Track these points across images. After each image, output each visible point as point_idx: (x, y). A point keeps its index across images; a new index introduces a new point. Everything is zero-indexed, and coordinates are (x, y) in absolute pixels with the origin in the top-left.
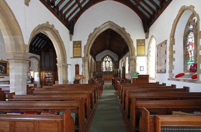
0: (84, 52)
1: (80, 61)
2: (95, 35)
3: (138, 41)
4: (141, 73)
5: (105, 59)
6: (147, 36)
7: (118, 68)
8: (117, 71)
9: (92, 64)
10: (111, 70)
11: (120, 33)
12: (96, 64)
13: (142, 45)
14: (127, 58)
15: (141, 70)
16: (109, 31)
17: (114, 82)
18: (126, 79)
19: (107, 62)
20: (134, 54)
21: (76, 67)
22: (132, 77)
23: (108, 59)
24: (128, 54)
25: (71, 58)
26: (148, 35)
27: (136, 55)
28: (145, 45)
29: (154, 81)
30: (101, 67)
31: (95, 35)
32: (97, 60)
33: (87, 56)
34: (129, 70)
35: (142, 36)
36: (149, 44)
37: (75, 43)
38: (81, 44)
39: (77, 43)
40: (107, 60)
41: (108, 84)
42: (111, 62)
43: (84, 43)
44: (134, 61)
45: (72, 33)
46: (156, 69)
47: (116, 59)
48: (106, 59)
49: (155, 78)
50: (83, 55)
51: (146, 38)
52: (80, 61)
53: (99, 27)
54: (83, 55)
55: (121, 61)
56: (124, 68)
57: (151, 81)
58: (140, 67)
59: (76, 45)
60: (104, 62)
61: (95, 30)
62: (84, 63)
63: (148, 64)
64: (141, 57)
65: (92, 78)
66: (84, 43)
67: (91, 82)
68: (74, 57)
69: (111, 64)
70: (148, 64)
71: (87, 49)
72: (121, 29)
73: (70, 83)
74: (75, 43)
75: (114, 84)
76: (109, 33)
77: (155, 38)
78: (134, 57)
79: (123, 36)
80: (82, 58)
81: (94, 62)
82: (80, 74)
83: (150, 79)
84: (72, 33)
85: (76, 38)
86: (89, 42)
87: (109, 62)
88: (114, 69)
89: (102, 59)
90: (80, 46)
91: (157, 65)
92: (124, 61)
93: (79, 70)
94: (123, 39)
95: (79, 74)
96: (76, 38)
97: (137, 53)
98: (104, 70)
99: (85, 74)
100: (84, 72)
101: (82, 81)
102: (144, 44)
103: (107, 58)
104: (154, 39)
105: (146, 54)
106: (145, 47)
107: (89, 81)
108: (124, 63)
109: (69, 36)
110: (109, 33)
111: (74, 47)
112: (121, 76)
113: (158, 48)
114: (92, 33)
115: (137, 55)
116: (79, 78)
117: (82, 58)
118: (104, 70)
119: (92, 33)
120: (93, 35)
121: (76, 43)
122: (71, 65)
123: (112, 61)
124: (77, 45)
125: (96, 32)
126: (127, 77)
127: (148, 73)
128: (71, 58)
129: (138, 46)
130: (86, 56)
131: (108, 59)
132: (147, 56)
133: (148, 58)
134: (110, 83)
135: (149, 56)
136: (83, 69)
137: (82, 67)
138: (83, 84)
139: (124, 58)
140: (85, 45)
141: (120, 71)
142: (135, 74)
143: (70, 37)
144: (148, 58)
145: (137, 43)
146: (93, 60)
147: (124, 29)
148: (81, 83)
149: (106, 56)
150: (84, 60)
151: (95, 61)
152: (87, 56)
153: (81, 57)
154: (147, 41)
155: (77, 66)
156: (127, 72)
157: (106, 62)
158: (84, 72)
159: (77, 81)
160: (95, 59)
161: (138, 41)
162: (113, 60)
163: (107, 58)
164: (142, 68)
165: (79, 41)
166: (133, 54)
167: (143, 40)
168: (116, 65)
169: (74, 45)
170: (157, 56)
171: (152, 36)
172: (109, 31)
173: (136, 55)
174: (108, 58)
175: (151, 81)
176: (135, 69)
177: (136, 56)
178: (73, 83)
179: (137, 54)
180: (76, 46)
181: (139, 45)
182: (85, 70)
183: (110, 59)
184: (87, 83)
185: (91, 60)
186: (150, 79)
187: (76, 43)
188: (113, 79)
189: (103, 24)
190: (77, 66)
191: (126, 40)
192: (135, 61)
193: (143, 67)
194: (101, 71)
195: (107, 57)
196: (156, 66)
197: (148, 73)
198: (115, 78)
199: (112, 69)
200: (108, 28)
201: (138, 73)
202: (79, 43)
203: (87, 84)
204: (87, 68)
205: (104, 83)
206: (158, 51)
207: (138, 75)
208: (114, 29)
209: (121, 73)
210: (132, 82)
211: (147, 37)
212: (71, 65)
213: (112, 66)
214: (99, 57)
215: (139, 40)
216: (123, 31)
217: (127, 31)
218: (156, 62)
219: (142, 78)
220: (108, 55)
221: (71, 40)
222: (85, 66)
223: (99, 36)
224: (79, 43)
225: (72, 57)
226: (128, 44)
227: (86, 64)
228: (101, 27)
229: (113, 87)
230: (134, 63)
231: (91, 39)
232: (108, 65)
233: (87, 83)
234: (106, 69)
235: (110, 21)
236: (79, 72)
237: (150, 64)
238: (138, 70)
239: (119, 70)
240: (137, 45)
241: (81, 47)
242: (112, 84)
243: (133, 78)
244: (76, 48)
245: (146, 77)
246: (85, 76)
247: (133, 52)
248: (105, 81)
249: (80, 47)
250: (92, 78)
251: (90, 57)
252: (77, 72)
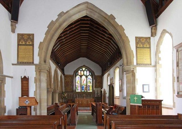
0: (39, 55)
1: (30, 72)
2: (60, 26)
3: (138, 40)
4: (149, 96)
5: (79, 72)
6: (153, 31)
7: (101, 87)
8: (99, 92)
9: (57, 79)
10: (89, 90)
11: (106, 25)
12: (65, 79)
13: (145, 48)
14: (117, 71)
15: (145, 90)
16: (88, 20)
17: (94, 110)
18: (116, 106)
19: (84, 77)
20: (131, 62)
21: (22, 81)
22: (131, 104)
23: (85, 72)
24: (118, 64)
25: (13, 64)
26: (156, 29)
27: (135, 64)
28: (150, 48)
29: (173, 113)
30: (73, 85)
31: (60, 26)
32: (66, 73)
33: (45, 62)
34: (121, 90)
35: (145, 31)
36: (158, 46)
37: (21, 37)
38: (33, 40)
39: (26, 38)
40: (82, 74)
41: (85, 113)
42: (90, 77)
43: (39, 39)
44: (131, 74)
45: (15, 17)
46: (174, 90)
47: (98, 73)
48: (82, 72)
49: (174, 106)
50: (37, 61)
51: (152, 36)
52: (30, 72)
53: (67, 12)
54: (37, 61)
55: (105, 76)
56: (111, 88)
57: (165, 112)
58: (143, 85)
59: (24, 40)
60: (79, 71)
61: (61, 15)
62: (40, 75)
63: (156, 81)
64: (104, 85)
65: (57, 102)
66: (39, 39)
67: (53, 111)
68: (19, 63)
69: (90, 80)
70: (156, 81)
71: (44, 50)
72: (107, 17)
73: (9, 111)
74: (21, 37)
75: (95, 114)
76: (86, 27)
77: (170, 34)
78: (132, 67)
79: (111, 30)
80: (34, 67)
81: (61, 76)
82: (31, 94)
83: (164, 107)
84: (15, 17)
85: (23, 28)
86: (49, 37)
87: (87, 77)
88: (94, 89)
89: (74, 72)
90: (31, 43)
91: (178, 81)
92: (112, 76)
93: (28, 88)
94: (110, 35)
95: (27, 95)
96: (23, 28)
97: (137, 60)
98: (79, 90)
99: (40, 96)
100: (38, 91)
101: (35, 110)
102: (148, 46)
103: (84, 71)
104: (167, 36)
105: (153, 63)
106: (150, 51)
107: (49, 109)
108: (112, 80)
109: (9, 23)
110: (86, 27)
111: (18, 45)
112: (107, 101)
113: (177, 51)
114: (54, 20)
115: (137, 64)
116: (27, 103)
117: (36, 65)
118: (79, 90)
119: (54, 20)
120: (57, 24)
121: (24, 37)
122: (12, 77)
123: (92, 76)
124: (26, 42)
125: (61, 20)
126: (117, 102)
127: (156, 97)
128: (13, 64)
129: (139, 48)
130: (43, 63)
131: (85, 72)
132: (155, 66)
133: (156, 70)
134: (88, 111)
135: (157, 68)
136: (36, 85)
137: (36, 81)
138: (36, 116)
139: (112, 70)
140: (41, 43)
141: (105, 91)
142: (136, 98)
143: (12, 25)
144: (156, 70)
145: (137, 43)
146: (59, 73)
147: (112, 17)
148: (33, 113)
149: (81, 67)
150: (39, 70)
151: (64, 74)
152: (45, 62)
153: (32, 63)
154: (154, 41)
155: (25, 80)
156: (117, 93)
157: (81, 76)
158: (38, 91)
159: (22, 110)
160: (63, 71)
161: (138, 40)
162: (92, 74)
163: (84, 71)
164: (146, 87)
165: (29, 35)
166: (129, 63)
167: (146, 38)
168: (98, 81)
169: (19, 41)
170: (178, 66)
171: (164, 31)
172: (88, 20)
173: (135, 64)
174: (85, 70)
175: (165, 112)
176: (134, 88)
177: (135, 67)
178: (15, 114)
179: (137, 62)
180: (24, 43)
181: (141, 48)
182: (40, 87)
183: (88, 72)
184: (44, 113)
185: (56, 71)
186: (164, 107)
187: (24, 37)
188: (95, 105)
189: (75, 7)
190: (25, 80)
191: (116, 37)
192: (134, 75)
193: (148, 85)
194: (73, 91)
195: (84, 69)
196: (176, 83)
197: (156, 97)
198: (97, 105)
199: (91, 88)
200: (83, 14)
201: (142, 97)
202: (29, 38)
203: (44, 116)
204: (44, 85)
205: (78, 112)
206: (178, 56)
207: (143, 100)
208: (95, 17)
209: (107, 95)
210: (128, 112)
211: (153, 34)
212: (12, 77)
213: (91, 85)
214: (69, 69)
215: (140, 38)
216: (112, 21)
217: (119, 21)
218: (174, 78)
219: (149, 106)
220: (84, 66)
221: (13, 31)
222: (40, 81)
223: (69, 26)
224: (29, 38)
225: (16, 63)
226: (121, 45)
227: (44, 78)
228: (71, 12)
229: (95, 120)
230: (132, 79)
231: (52, 32)
232: (85, 82)
233: (44, 113)
234: (82, 87)
235: (87, 3)
236: (28, 91)
237: (160, 80)
238: (139, 91)
239: (103, 90)
240: (137, 47)
241: (33, 45)
242: (92, 114)
243: (131, 106)
244: (23, 47)
245: (157, 104)
246: (40, 99)
247: (129, 59)
248: (79, 108)
249: (30, 45)
250: (57, 102)
251: (53, 66)
252: (25, 91)
